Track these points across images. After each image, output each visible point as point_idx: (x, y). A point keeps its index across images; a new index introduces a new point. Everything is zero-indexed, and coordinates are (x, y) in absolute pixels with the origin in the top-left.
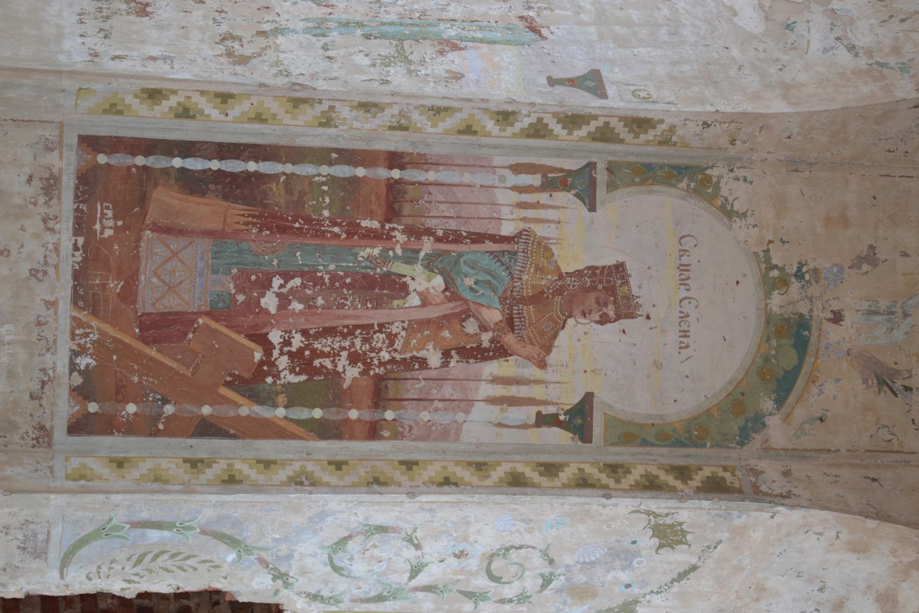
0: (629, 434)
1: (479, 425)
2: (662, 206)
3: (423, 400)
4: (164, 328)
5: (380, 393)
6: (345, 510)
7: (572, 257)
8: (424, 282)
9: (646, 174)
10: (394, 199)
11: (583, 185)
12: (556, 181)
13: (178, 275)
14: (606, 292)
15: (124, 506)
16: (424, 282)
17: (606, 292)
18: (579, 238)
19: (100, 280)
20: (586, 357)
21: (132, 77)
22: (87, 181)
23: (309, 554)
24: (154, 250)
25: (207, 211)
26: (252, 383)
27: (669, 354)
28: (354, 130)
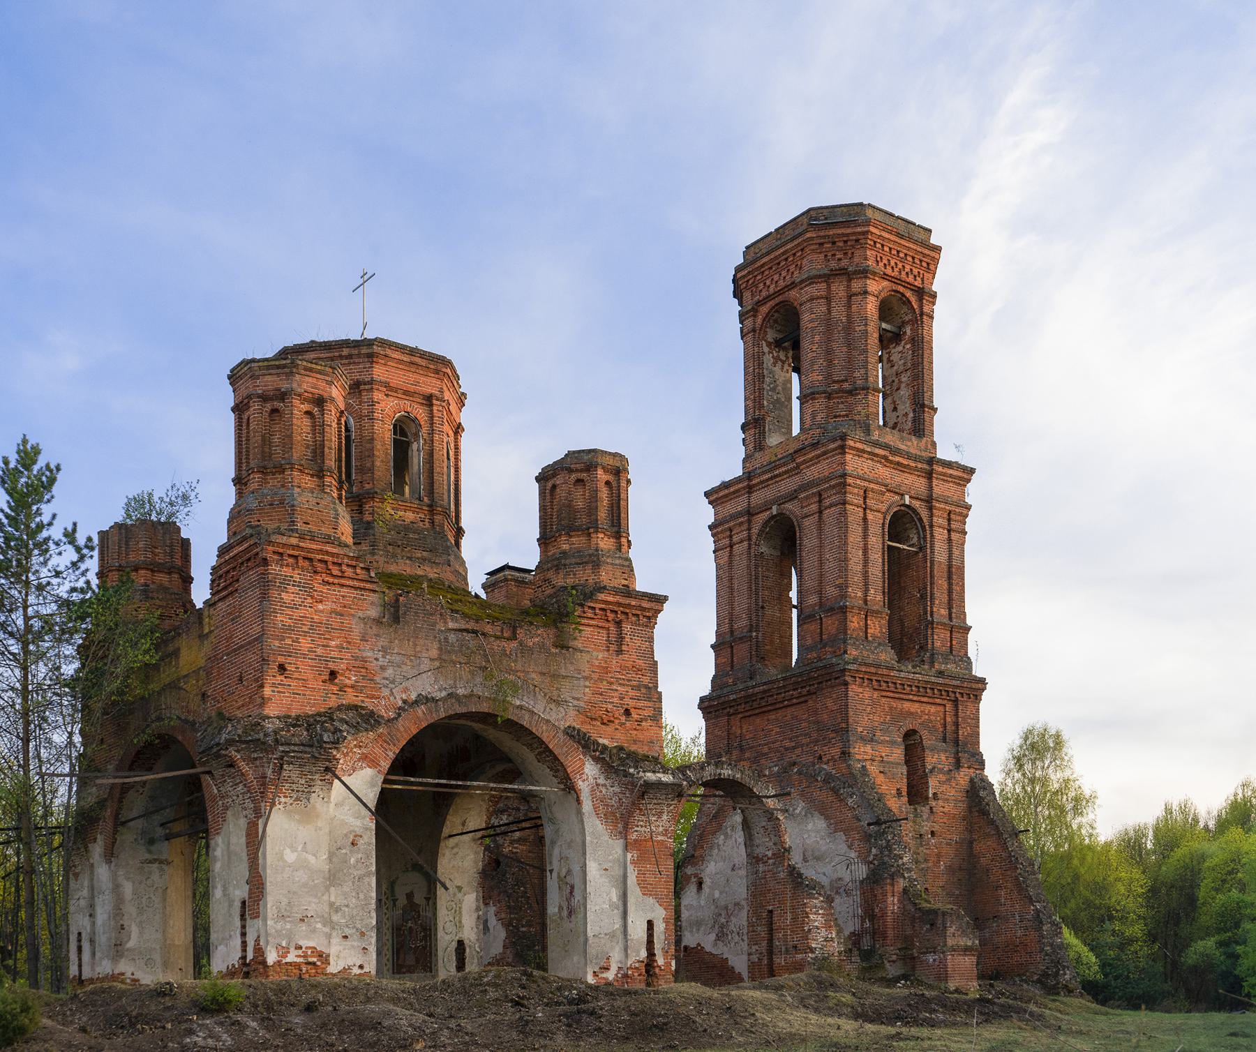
0: (429, 891)
1: (430, 914)
2: (397, 889)
3: (843, 588)
4: (417, 961)
5: (425, 929)
6: (440, 933)
8: (410, 924)
9: (393, 892)
10: (399, 929)
11: (395, 901)
12: (394, 905)
13: (410, 960)
14: (410, 896)
15: (440, 962)
16: (410, 924)
17: (410, 896)
18: (402, 901)
19: (411, 970)
20: (419, 899)
21: (731, 588)
22: (399, 973)
23: (448, 938)
24: (408, 963)
25: (402, 956)
26: (424, 948)
27: (415, 882)
28: (389, 936)
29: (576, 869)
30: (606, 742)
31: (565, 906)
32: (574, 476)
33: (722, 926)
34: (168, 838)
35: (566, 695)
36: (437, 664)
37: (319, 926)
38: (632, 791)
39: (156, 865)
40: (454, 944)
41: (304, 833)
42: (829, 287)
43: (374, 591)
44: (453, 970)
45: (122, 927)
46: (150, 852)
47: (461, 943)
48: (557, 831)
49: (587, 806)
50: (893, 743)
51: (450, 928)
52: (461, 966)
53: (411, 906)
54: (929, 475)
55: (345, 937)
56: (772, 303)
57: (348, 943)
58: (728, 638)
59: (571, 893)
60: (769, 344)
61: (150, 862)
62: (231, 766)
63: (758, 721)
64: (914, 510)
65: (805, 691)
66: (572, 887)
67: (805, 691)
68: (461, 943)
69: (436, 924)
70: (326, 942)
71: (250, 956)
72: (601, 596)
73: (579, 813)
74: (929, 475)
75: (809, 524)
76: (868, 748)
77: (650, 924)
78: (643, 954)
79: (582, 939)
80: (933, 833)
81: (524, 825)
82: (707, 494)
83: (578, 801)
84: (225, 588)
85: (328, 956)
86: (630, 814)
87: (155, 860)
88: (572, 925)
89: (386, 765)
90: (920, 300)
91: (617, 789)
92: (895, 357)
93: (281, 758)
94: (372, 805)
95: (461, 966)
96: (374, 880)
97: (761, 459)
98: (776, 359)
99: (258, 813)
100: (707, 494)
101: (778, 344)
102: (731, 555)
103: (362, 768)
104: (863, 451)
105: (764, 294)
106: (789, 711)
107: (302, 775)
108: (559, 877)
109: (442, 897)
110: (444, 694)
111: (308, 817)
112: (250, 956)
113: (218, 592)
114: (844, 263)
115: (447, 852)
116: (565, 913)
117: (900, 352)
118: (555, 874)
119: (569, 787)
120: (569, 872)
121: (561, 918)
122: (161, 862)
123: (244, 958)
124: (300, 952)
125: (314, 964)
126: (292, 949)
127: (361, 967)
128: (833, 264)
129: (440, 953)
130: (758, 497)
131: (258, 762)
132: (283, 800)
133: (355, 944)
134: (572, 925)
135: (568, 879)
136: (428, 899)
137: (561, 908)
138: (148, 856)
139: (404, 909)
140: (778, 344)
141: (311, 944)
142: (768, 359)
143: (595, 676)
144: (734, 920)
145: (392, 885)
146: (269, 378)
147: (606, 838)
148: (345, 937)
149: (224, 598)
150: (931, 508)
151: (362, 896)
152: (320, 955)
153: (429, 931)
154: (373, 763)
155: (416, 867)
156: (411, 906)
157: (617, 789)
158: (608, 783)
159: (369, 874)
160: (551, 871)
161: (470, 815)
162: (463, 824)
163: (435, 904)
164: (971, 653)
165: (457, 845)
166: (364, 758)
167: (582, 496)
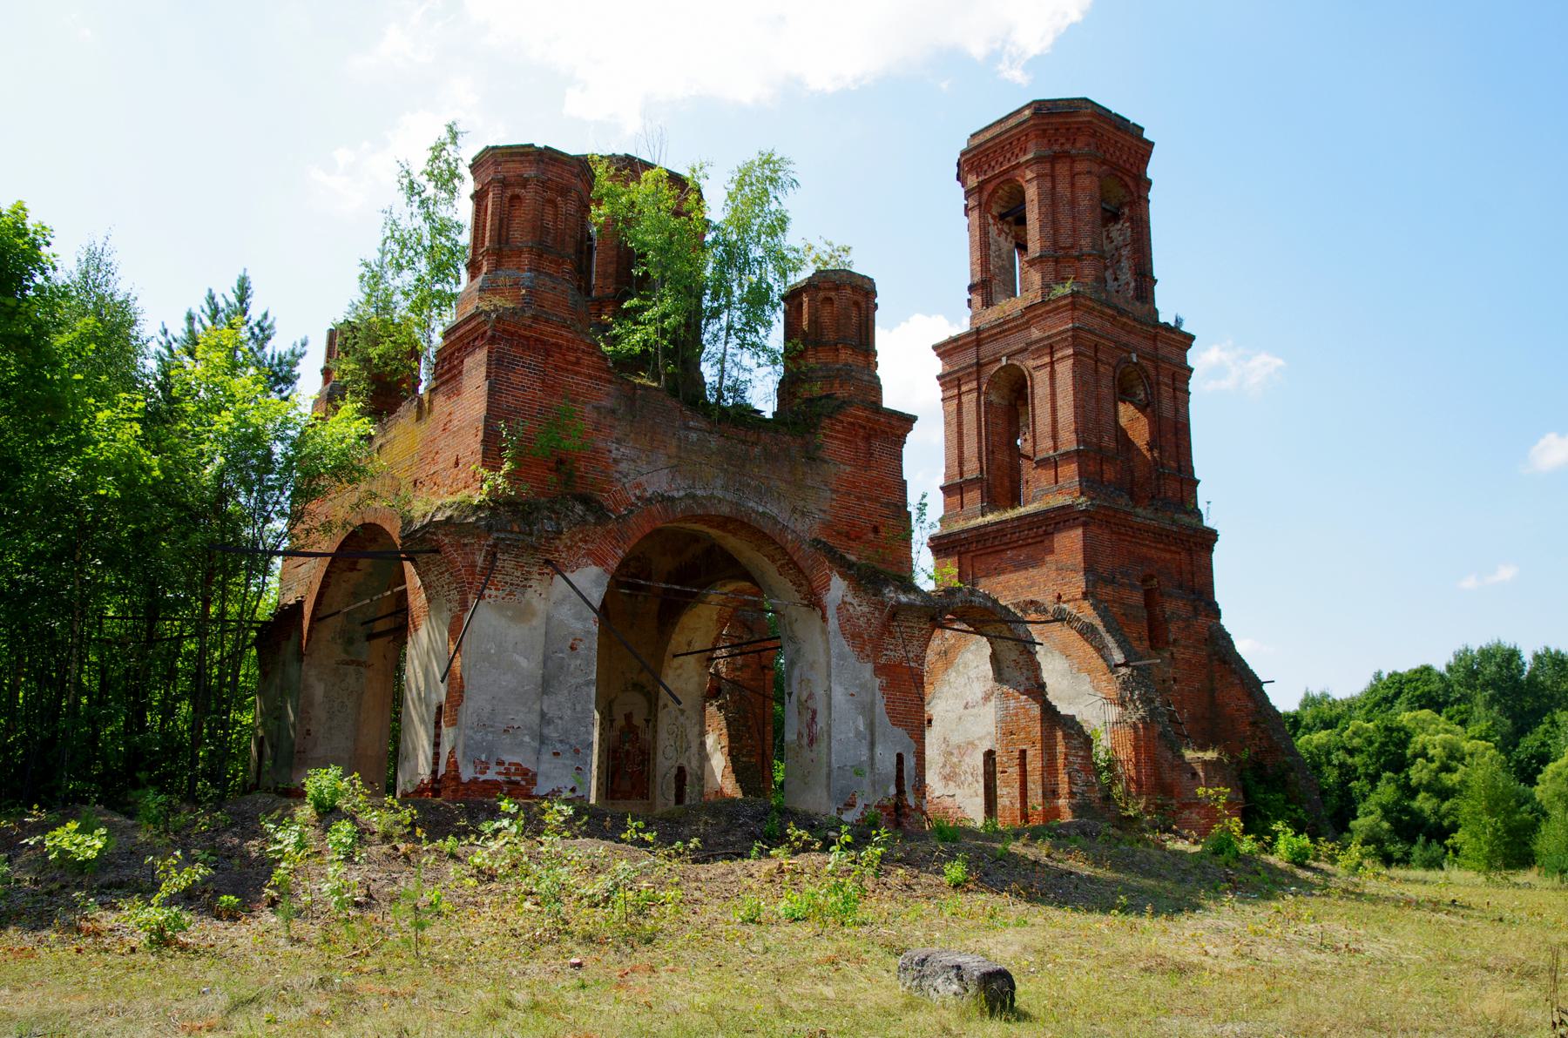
1: (648, 737)
4: (634, 787)
5: (643, 752)
6: (660, 758)
7: (623, 722)
8: (627, 746)
9: (610, 710)
10: (615, 751)
11: (612, 721)
14: (628, 717)
15: (658, 792)
16: (627, 746)
17: (628, 717)
18: (620, 722)
19: (627, 796)
20: (638, 721)
23: (668, 763)
26: (642, 773)
29: (819, 692)
30: (853, 558)
31: (805, 732)
32: (821, 294)
33: (954, 766)
34: (371, 637)
35: (812, 507)
36: (675, 461)
37: (527, 739)
38: (882, 612)
39: (352, 668)
40: (674, 771)
41: (515, 632)
42: (1053, 168)
43: (610, 382)
44: (672, 803)
45: (308, 732)
46: (347, 652)
47: (681, 770)
48: (798, 651)
49: (833, 623)
50: (1133, 586)
51: (670, 752)
52: (680, 798)
53: (630, 729)
54: (1154, 338)
55: (556, 754)
56: (994, 183)
57: (559, 761)
58: (957, 480)
59: (813, 718)
60: (994, 217)
61: (347, 663)
62: (437, 551)
63: (990, 559)
64: (1142, 368)
65: (1041, 531)
66: (814, 712)
67: (1041, 531)
68: (681, 770)
69: (655, 748)
70: (534, 758)
71: (442, 770)
72: (851, 410)
73: (825, 632)
74: (1154, 338)
75: (1041, 377)
76: (1109, 589)
77: (900, 757)
78: (893, 790)
79: (824, 771)
80: (1175, 680)
81: (746, 648)
82: (935, 348)
83: (824, 618)
84: (449, 370)
85: (535, 775)
86: (880, 637)
87: (352, 662)
88: (813, 755)
89: (614, 564)
90: (1138, 185)
91: (865, 609)
92: (1114, 234)
93: (495, 545)
94: (597, 604)
95: (680, 798)
96: (594, 690)
97: (992, 315)
98: (1001, 231)
99: (464, 606)
100: (935, 348)
101: (1002, 217)
102: (960, 405)
103: (587, 565)
104: (1093, 309)
105: (990, 174)
106: (1025, 551)
107: (519, 566)
108: (799, 700)
109: (665, 720)
110: (682, 493)
111: (523, 614)
112: (442, 770)
113: (441, 375)
114: (1067, 147)
115: (670, 673)
116: (805, 741)
117: (1120, 232)
118: (794, 698)
119: (814, 602)
120: (811, 696)
121: (801, 746)
122: (359, 664)
123: (435, 772)
124: (502, 769)
125: (517, 783)
126: (493, 765)
127: (573, 790)
128: (1056, 148)
129: (659, 779)
130: (987, 350)
131: (468, 549)
132: (494, 593)
133: (568, 762)
134: (813, 755)
135: (810, 703)
136: (647, 721)
137: (800, 735)
138: (344, 656)
139: (622, 730)
140: (1002, 217)
141: (516, 760)
142: (993, 231)
143: (843, 489)
144: (967, 759)
145: (610, 704)
146: (511, 165)
147: (852, 659)
148: (556, 754)
149: (447, 381)
150: (1156, 368)
151: (579, 708)
152: (525, 773)
153: (646, 756)
154: (600, 561)
155: (638, 687)
156: (630, 729)
157: (865, 609)
158: (855, 602)
159: (588, 684)
160: (790, 694)
161: (702, 623)
162: (689, 644)
163: (655, 726)
164: (1201, 506)
165: (681, 666)
166: (590, 554)
167: (835, 315)
